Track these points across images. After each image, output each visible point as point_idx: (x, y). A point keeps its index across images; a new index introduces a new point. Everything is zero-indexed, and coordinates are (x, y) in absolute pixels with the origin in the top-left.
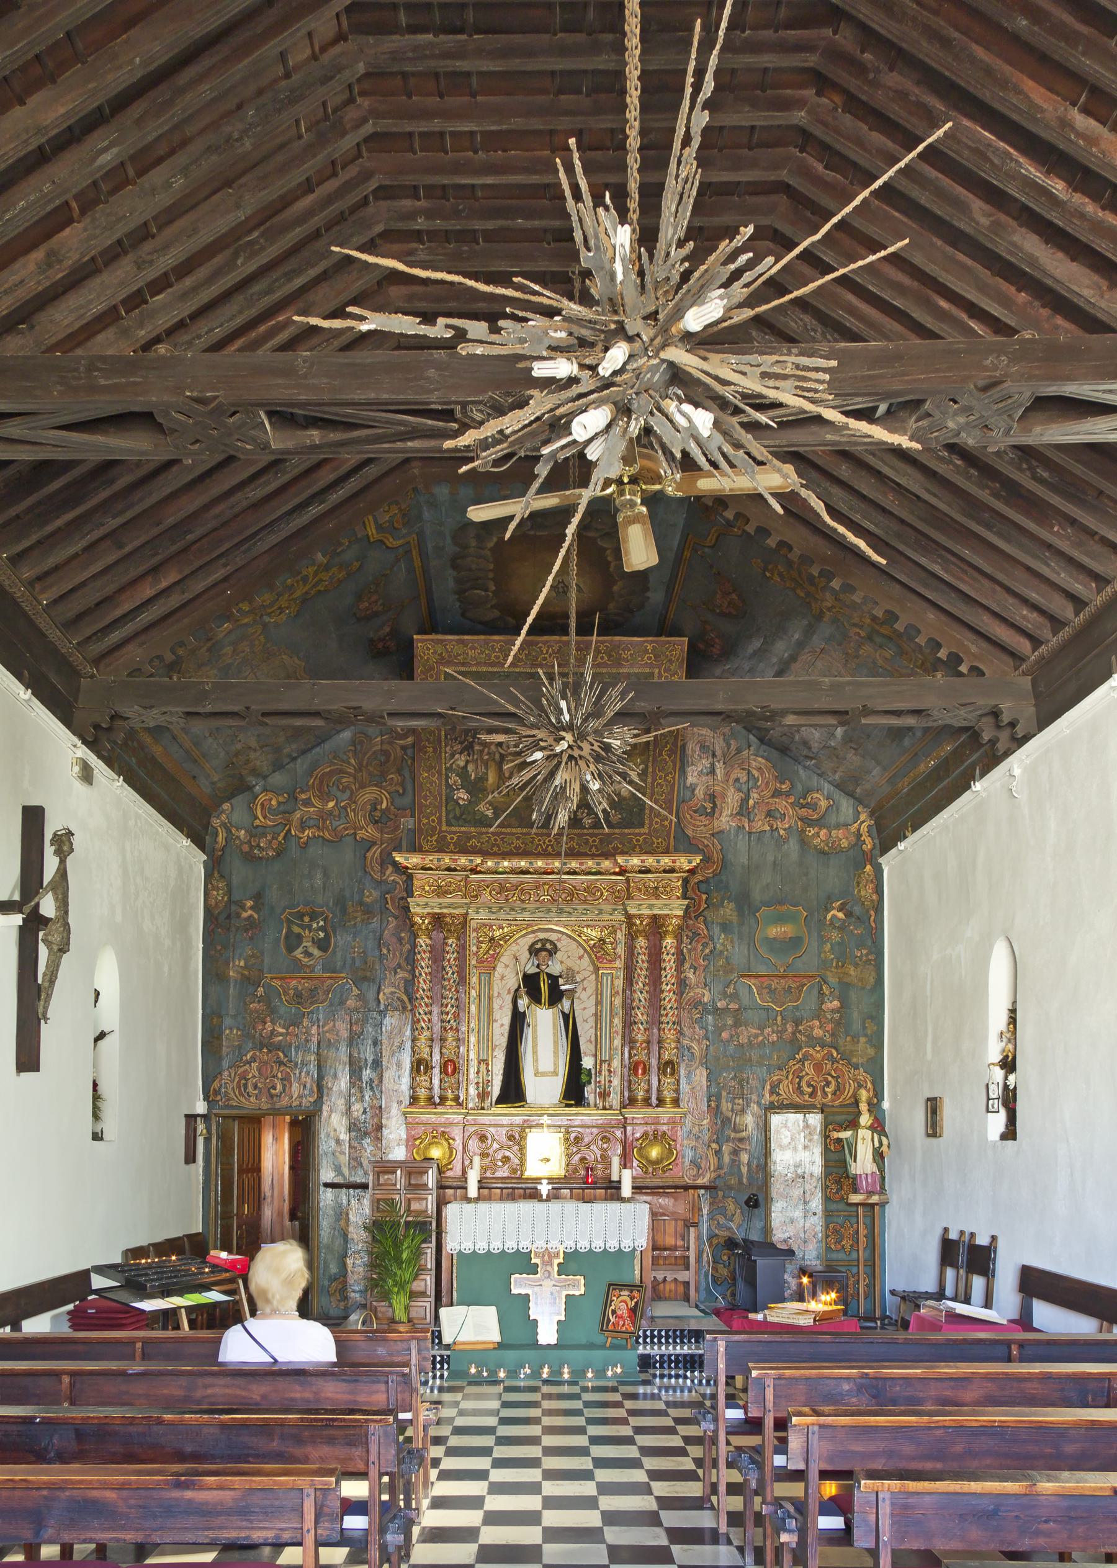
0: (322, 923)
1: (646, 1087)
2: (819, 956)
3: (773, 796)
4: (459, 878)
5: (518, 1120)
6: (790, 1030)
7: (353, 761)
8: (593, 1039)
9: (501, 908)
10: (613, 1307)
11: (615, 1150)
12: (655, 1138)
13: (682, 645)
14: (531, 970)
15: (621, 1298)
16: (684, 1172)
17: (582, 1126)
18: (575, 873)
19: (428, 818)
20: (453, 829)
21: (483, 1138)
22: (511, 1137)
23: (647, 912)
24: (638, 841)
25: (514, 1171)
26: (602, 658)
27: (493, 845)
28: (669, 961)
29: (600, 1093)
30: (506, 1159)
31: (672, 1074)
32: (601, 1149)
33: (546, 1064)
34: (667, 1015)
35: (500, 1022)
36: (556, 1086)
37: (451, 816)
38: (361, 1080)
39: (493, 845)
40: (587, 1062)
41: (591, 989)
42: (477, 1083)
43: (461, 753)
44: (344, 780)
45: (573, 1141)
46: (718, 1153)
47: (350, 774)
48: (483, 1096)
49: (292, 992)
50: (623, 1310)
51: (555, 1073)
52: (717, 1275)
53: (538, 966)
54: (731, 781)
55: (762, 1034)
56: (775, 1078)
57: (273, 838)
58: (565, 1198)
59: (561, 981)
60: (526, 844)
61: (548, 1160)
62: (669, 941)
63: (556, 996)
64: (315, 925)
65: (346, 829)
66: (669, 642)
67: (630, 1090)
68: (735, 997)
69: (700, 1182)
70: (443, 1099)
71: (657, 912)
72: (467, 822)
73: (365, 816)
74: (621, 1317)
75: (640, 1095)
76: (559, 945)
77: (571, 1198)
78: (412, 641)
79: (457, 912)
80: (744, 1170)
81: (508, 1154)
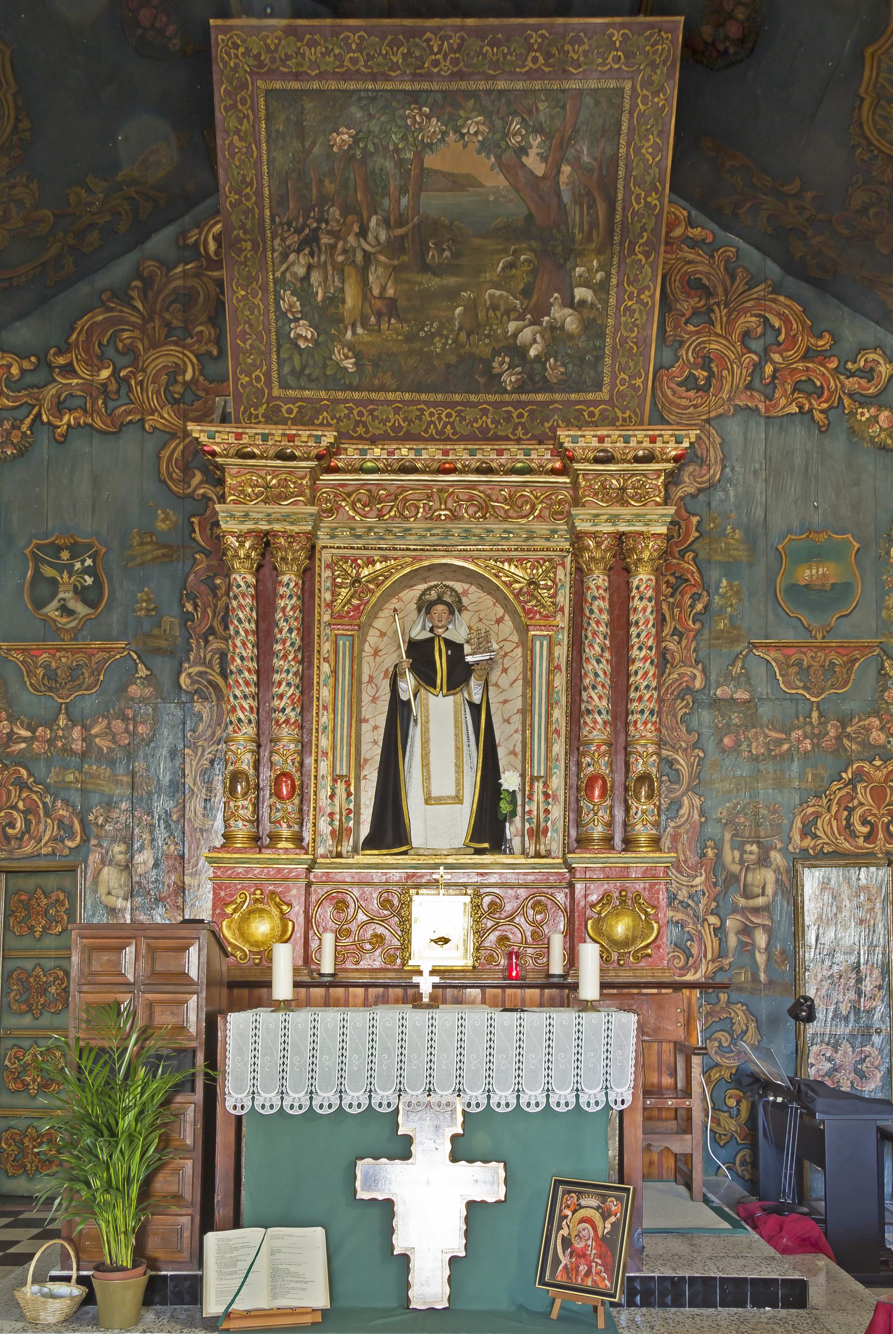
0: (89, 562)
1: (607, 818)
2: (878, 614)
3: (805, 358)
4: (301, 473)
5: (396, 875)
6: (832, 733)
7: (139, 305)
8: (519, 749)
9: (370, 529)
10: (565, 1232)
11: (556, 925)
12: (623, 902)
13: (673, 31)
14: (419, 633)
15: (582, 1213)
16: (666, 964)
17: (503, 885)
18: (489, 471)
19: (249, 375)
20: (290, 393)
21: (341, 905)
22: (385, 903)
23: (607, 528)
24: (591, 414)
25: (392, 959)
26: (535, 60)
27: (357, 423)
28: (644, 609)
29: (531, 830)
30: (378, 939)
31: (650, 797)
32: (533, 923)
33: (443, 786)
34: (640, 699)
35: (372, 722)
36: (460, 819)
37: (286, 369)
38: (150, 813)
39: (357, 423)
40: (510, 781)
41: (516, 668)
42: (331, 815)
43: (299, 251)
44: (125, 335)
45: (485, 912)
46: (719, 931)
47: (134, 325)
48: (338, 835)
49: (40, 672)
50: (586, 1241)
51: (458, 799)
52: (719, 1130)
53: (431, 630)
54: (735, 336)
55: (788, 740)
56: (810, 810)
57: (13, 427)
58: (473, 1002)
59: (467, 649)
60: (410, 422)
61: (446, 941)
62: (643, 577)
63: (460, 674)
64: (78, 566)
65: (129, 413)
66: (651, 26)
67: (579, 824)
68: (745, 679)
69: (689, 977)
70: (275, 838)
71: (623, 528)
72: (313, 382)
73: (158, 393)
74: (582, 1255)
75: (598, 831)
76: (465, 601)
77: (483, 1002)
78: (207, 28)
79: (296, 528)
80: (761, 959)
81: (380, 930)
